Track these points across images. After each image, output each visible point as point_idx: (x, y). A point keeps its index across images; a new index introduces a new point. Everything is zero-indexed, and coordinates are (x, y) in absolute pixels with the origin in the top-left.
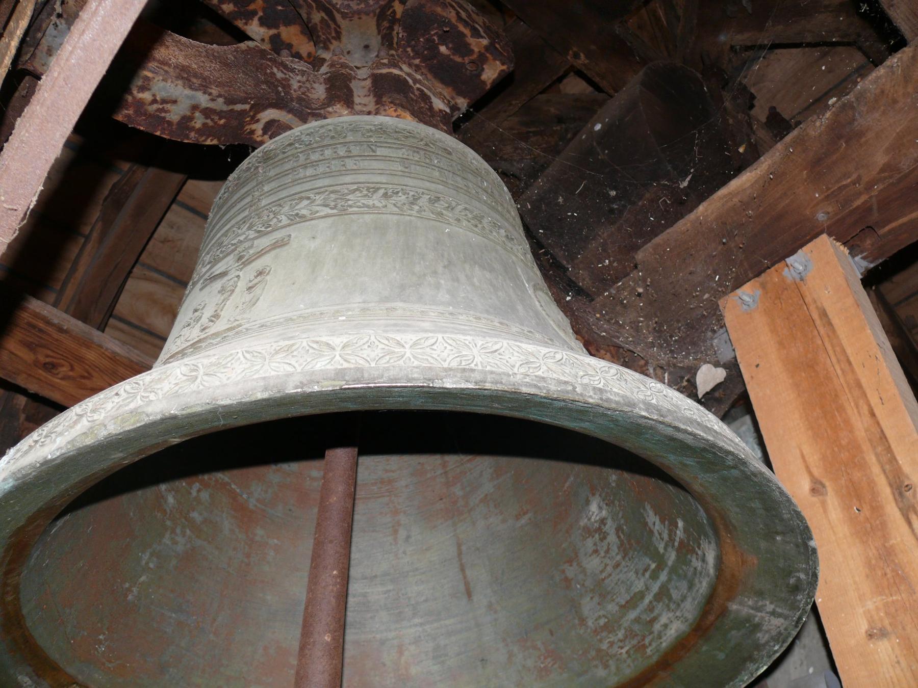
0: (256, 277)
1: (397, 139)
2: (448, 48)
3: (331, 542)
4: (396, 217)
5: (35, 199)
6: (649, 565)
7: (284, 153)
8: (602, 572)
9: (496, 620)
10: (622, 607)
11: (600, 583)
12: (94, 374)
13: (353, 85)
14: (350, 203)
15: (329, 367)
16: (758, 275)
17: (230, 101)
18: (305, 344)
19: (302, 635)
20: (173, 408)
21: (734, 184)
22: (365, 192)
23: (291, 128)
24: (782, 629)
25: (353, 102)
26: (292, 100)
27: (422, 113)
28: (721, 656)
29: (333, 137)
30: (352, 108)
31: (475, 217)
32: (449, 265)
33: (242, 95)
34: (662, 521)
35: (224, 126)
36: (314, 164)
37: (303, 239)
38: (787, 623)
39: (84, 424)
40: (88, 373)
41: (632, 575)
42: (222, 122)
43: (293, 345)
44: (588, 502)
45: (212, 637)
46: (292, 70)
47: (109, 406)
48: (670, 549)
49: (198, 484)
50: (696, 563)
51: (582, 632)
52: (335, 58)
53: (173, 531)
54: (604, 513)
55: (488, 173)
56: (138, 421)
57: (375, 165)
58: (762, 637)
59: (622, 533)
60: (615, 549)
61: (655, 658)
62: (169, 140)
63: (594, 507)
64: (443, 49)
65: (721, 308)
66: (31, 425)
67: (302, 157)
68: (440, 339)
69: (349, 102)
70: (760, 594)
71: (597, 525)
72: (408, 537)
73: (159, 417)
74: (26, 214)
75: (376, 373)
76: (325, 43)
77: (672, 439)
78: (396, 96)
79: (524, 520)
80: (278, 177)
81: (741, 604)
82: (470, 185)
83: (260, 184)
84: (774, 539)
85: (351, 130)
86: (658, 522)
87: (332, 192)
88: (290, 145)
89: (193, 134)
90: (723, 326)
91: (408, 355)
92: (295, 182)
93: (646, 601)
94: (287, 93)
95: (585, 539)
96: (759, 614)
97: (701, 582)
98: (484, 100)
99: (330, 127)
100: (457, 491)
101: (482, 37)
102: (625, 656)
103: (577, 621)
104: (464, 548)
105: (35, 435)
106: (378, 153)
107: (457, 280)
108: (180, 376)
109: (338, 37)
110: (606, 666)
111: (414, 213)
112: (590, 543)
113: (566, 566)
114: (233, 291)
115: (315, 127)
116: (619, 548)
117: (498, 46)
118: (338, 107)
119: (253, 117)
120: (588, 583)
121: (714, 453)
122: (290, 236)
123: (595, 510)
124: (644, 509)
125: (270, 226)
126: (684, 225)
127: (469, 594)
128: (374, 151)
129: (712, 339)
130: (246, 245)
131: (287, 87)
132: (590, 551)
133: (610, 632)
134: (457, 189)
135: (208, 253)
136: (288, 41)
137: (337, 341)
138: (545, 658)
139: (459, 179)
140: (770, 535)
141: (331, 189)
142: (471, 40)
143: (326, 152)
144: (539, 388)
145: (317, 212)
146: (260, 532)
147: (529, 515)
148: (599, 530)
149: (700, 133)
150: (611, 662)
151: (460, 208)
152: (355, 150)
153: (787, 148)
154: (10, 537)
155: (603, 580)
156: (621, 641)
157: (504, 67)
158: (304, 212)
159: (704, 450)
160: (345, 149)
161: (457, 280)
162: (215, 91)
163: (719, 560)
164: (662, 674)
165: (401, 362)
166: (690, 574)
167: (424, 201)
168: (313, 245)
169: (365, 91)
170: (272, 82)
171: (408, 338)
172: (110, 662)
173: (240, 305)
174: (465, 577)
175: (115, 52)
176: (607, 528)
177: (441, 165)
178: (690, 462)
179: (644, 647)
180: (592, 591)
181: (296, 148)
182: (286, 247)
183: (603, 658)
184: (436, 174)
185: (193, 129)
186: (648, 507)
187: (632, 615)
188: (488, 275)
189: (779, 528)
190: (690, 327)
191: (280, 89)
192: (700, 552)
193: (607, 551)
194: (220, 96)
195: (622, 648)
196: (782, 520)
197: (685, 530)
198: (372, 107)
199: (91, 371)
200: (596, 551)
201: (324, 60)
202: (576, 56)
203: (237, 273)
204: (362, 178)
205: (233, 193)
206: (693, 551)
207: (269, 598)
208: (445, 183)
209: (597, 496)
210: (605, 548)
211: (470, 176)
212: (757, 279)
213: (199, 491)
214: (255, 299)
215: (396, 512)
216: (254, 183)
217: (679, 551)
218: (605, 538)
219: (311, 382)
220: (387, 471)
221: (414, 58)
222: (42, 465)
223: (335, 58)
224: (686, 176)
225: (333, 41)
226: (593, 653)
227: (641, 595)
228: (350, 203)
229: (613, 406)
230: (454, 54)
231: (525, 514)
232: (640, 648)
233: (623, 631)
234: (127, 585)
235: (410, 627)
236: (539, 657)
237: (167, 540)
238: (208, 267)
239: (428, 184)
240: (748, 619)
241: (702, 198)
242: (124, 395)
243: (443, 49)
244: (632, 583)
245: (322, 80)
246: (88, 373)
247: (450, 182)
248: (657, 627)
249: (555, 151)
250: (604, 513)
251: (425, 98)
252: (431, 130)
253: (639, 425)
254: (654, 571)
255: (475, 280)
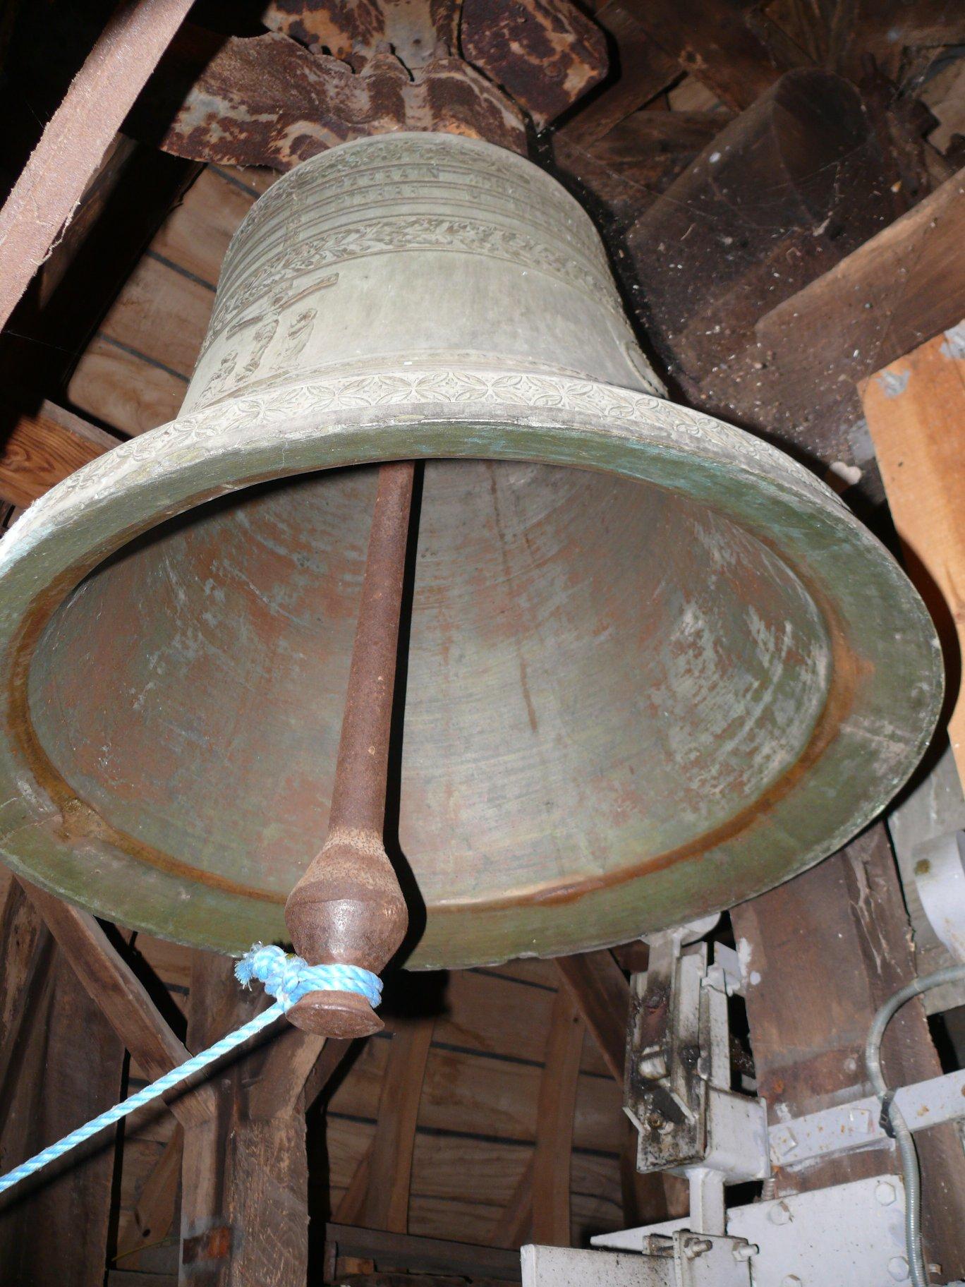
0: (299, 321)
1: (464, 162)
2: (521, 45)
3: (376, 643)
4: (463, 256)
5: (71, 215)
6: (751, 684)
7: (324, 176)
8: (695, 695)
9: (565, 756)
10: (717, 737)
11: (692, 709)
12: (56, 465)
13: (406, 92)
14: (408, 237)
15: (405, 401)
16: (909, 351)
17: (254, 110)
18: (376, 379)
19: (342, 748)
20: (237, 443)
21: (887, 235)
22: (426, 225)
23: (327, 148)
24: (902, 757)
25: (404, 115)
26: (328, 110)
27: (490, 130)
28: (832, 793)
29: (384, 158)
30: (404, 122)
31: (557, 260)
32: (527, 312)
33: (270, 102)
34: (768, 627)
35: (245, 141)
36: (363, 191)
37: (351, 278)
38: (908, 749)
39: (130, 466)
40: (48, 463)
41: (730, 697)
42: (243, 136)
43: (363, 381)
44: (681, 612)
45: (227, 763)
46: (328, 72)
47: (159, 444)
48: (776, 662)
49: (211, 580)
50: (806, 677)
51: (668, 768)
52: (381, 57)
53: (184, 634)
54: (700, 623)
55: (573, 208)
56: (196, 457)
57: (437, 193)
58: (880, 768)
59: (722, 646)
60: (712, 667)
61: (754, 798)
62: (178, 158)
63: (688, 618)
64: (515, 47)
65: (860, 392)
66: (41, 488)
67: (347, 182)
68: (524, 378)
69: (398, 113)
70: (878, 712)
71: (691, 639)
72: (461, 656)
73: (221, 451)
74: (60, 232)
75: (456, 409)
76: (364, 36)
77: (776, 502)
78: (458, 108)
79: (603, 637)
80: (317, 205)
81: (856, 725)
82: (551, 221)
83: (298, 214)
84: (893, 638)
85: (407, 150)
86: (763, 628)
87: (386, 224)
88: (332, 166)
89: (207, 151)
90: (861, 416)
91: (490, 392)
92: (341, 211)
93: (747, 728)
94: (322, 101)
95: (676, 656)
96: (877, 738)
97: (810, 700)
98: (571, 114)
99: (381, 146)
100: (523, 602)
101: (567, 31)
102: (718, 796)
103: (663, 757)
104: (529, 670)
105: (68, 482)
106: (441, 179)
107: (537, 330)
108: (238, 412)
109: (381, 28)
110: (696, 809)
111: (485, 251)
112: (682, 661)
113: (652, 691)
114: (272, 338)
115: (361, 145)
116: (716, 665)
117: (587, 44)
118: (386, 121)
119: (280, 132)
120: (679, 710)
121: (823, 522)
122: (337, 275)
123: (690, 621)
124: (748, 614)
125: (311, 263)
126: (818, 287)
127: (534, 724)
128: (435, 176)
129: (846, 432)
130: (284, 285)
131: (322, 93)
132: (682, 670)
133: (702, 768)
134: (535, 225)
135: (232, 297)
136: (313, 32)
137: (412, 377)
138: (624, 801)
139: (538, 214)
140: (887, 634)
141: (385, 220)
142: (552, 36)
143: (377, 176)
144: (631, 431)
145: (369, 247)
146: (283, 643)
147: (610, 630)
148: (693, 645)
149: (842, 165)
150: (702, 805)
151: (539, 248)
152: (413, 175)
153: (957, 189)
154: (32, 602)
155: (696, 705)
156: (714, 778)
157: (594, 73)
158: (352, 247)
159: (812, 516)
160: (400, 172)
161: (537, 330)
162: (236, 97)
163: (832, 668)
164: (761, 817)
165: (483, 399)
166: (798, 690)
167: (497, 237)
168: (366, 285)
169: (419, 102)
170: (304, 88)
171: (490, 376)
172: (114, 779)
173: (283, 354)
174: (529, 705)
175: (165, 47)
176: (701, 643)
177: (517, 196)
178: (795, 533)
179: (742, 784)
180: (683, 719)
181: (339, 171)
182: (334, 288)
183: (693, 800)
184: (511, 206)
185: (207, 144)
186: (752, 611)
187: (729, 746)
188: (572, 327)
189: (899, 623)
190: (819, 416)
191: (313, 95)
192: (810, 662)
193: (702, 671)
194: (243, 102)
195: (715, 786)
196: (901, 612)
197: (795, 636)
198: (428, 121)
199: (51, 460)
200: (689, 671)
201: (363, 60)
202: (691, 58)
203: (275, 318)
204: (422, 208)
205: (260, 226)
206: (803, 662)
207: (293, 721)
208: (522, 218)
209: (693, 603)
210: (700, 666)
211: (552, 211)
212: (907, 356)
213: (213, 589)
214: (300, 346)
215: (446, 627)
216: (287, 213)
217: (786, 662)
218: (700, 654)
219: (388, 416)
220: (436, 577)
221: (476, 58)
222: (87, 506)
223: (381, 57)
224: (822, 220)
225: (375, 33)
226: (681, 794)
227: (741, 721)
228: (408, 237)
229: (711, 455)
230: (529, 54)
231: (605, 628)
232: (738, 786)
233: (717, 766)
234: (133, 691)
235: (462, 763)
236: (616, 800)
237: (176, 643)
238: (235, 312)
239: (500, 219)
240: (864, 745)
241: (845, 251)
242: (174, 434)
243: (515, 47)
244: (730, 708)
245: (364, 85)
246: (48, 463)
247: (527, 216)
248: (758, 759)
249: (653, 189)
250: (700, 623)
251: (495, 112)
252: (504, 153)
253: (739, 482)
254: (756, 691)
255: (557, 331)
